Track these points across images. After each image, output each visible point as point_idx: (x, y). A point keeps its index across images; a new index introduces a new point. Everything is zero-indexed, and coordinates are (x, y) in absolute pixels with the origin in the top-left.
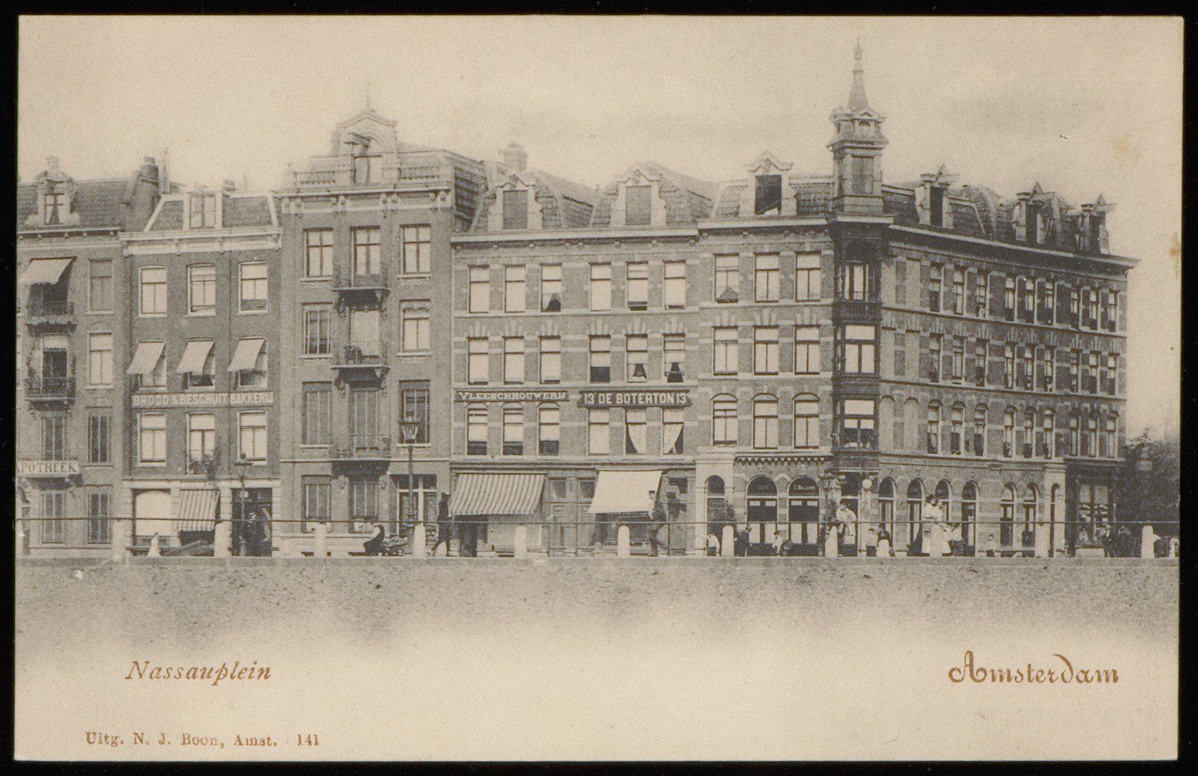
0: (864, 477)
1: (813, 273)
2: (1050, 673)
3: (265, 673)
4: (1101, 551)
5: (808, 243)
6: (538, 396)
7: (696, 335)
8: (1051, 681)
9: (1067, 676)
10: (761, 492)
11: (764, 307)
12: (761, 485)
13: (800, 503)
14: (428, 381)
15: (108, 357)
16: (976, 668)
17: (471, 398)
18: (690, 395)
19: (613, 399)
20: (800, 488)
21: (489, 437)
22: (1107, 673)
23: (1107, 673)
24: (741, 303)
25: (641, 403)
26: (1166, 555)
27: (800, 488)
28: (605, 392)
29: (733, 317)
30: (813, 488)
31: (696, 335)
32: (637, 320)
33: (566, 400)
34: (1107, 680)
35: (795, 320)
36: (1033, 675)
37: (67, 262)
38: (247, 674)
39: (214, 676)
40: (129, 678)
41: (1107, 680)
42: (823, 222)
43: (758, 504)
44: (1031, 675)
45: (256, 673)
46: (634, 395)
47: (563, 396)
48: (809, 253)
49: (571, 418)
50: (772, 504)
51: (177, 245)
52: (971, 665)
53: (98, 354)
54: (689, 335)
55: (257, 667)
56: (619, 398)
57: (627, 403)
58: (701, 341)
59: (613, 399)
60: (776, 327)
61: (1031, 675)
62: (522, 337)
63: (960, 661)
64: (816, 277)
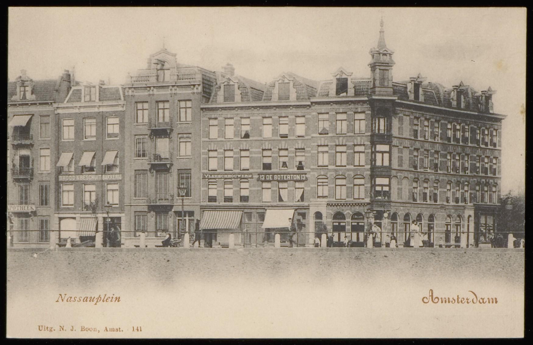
0: (384, 212)
2: (467, 299)
3: (118, 299)
4: (490, 245)
5: (360, 108)
6: (239, 176)
7: (310, 149)
8: (468, 303)
9: (475, 300)
10: (338, 219)
12: (339, 216)
13: (356, 224)
16: (434, 297)
18: (307, 176)
19: (273, 177)
20: (356, 217)
22: (492, 299)
23: (492, 299)
24: (330, 135)
25: (285, 179)
27: (356, 217)
28: (269, 174)
30: (362, 217)
31: (310, 149)
32: (283, 142)
33: (252, 178)
34: (493, 302)
36: (460, 300)
37: (30, 116)
38: (110, 299)
39: (95, 300)
40: (57, 301)
41: (493, 302)
44: (459, 300)
45: (114, 299)
46: (282, 175)
47: (250, 176)
49: (254, 186)
50: (344, 224)
52: (432, 296)
54: (306, 149)
55: (114, 297)
57: (279, 179)
58: (312, 152)
59: (273, 177)
60: (345, 145)
61: (459, 300)
62: (232, 150)
63: (427, 294)
64: (363, 123)
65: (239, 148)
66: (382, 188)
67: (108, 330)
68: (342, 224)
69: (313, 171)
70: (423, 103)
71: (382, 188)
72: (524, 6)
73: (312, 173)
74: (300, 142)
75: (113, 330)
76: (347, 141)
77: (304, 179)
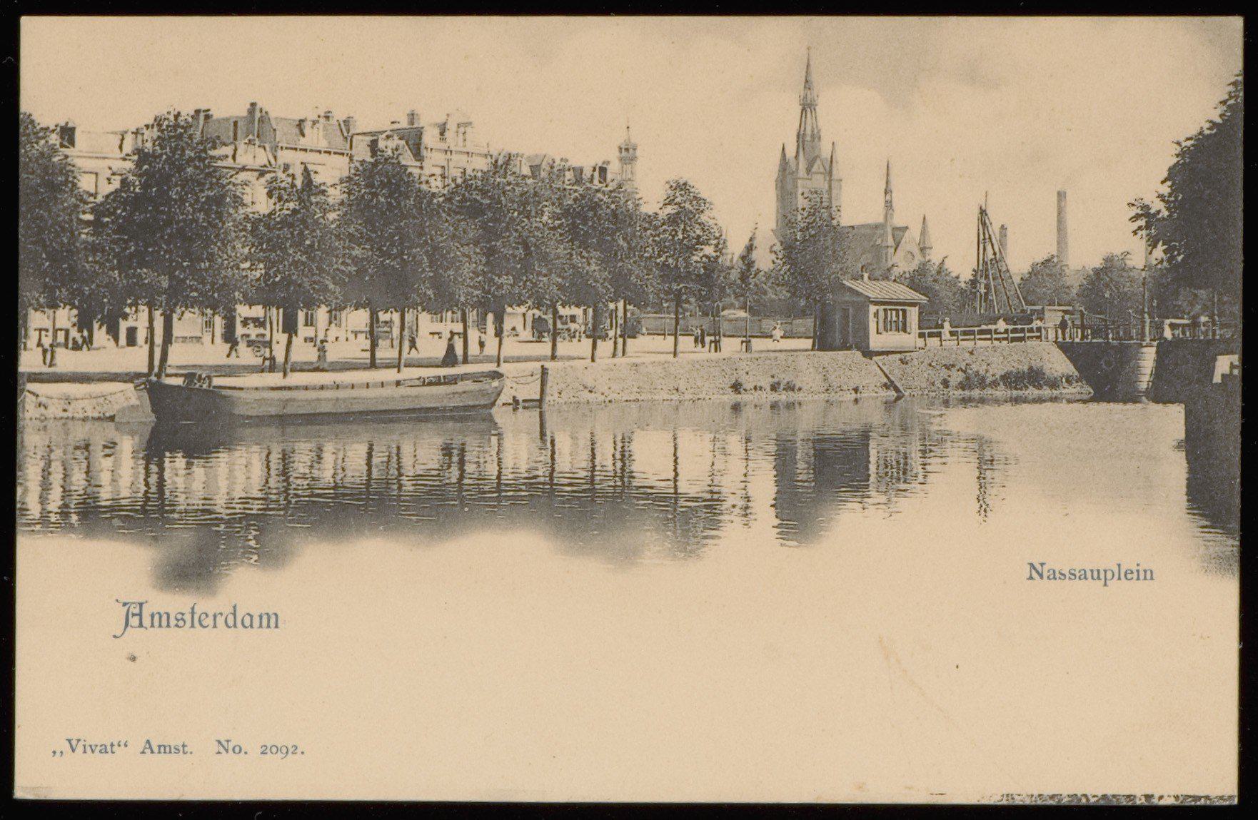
67: (156, 749)
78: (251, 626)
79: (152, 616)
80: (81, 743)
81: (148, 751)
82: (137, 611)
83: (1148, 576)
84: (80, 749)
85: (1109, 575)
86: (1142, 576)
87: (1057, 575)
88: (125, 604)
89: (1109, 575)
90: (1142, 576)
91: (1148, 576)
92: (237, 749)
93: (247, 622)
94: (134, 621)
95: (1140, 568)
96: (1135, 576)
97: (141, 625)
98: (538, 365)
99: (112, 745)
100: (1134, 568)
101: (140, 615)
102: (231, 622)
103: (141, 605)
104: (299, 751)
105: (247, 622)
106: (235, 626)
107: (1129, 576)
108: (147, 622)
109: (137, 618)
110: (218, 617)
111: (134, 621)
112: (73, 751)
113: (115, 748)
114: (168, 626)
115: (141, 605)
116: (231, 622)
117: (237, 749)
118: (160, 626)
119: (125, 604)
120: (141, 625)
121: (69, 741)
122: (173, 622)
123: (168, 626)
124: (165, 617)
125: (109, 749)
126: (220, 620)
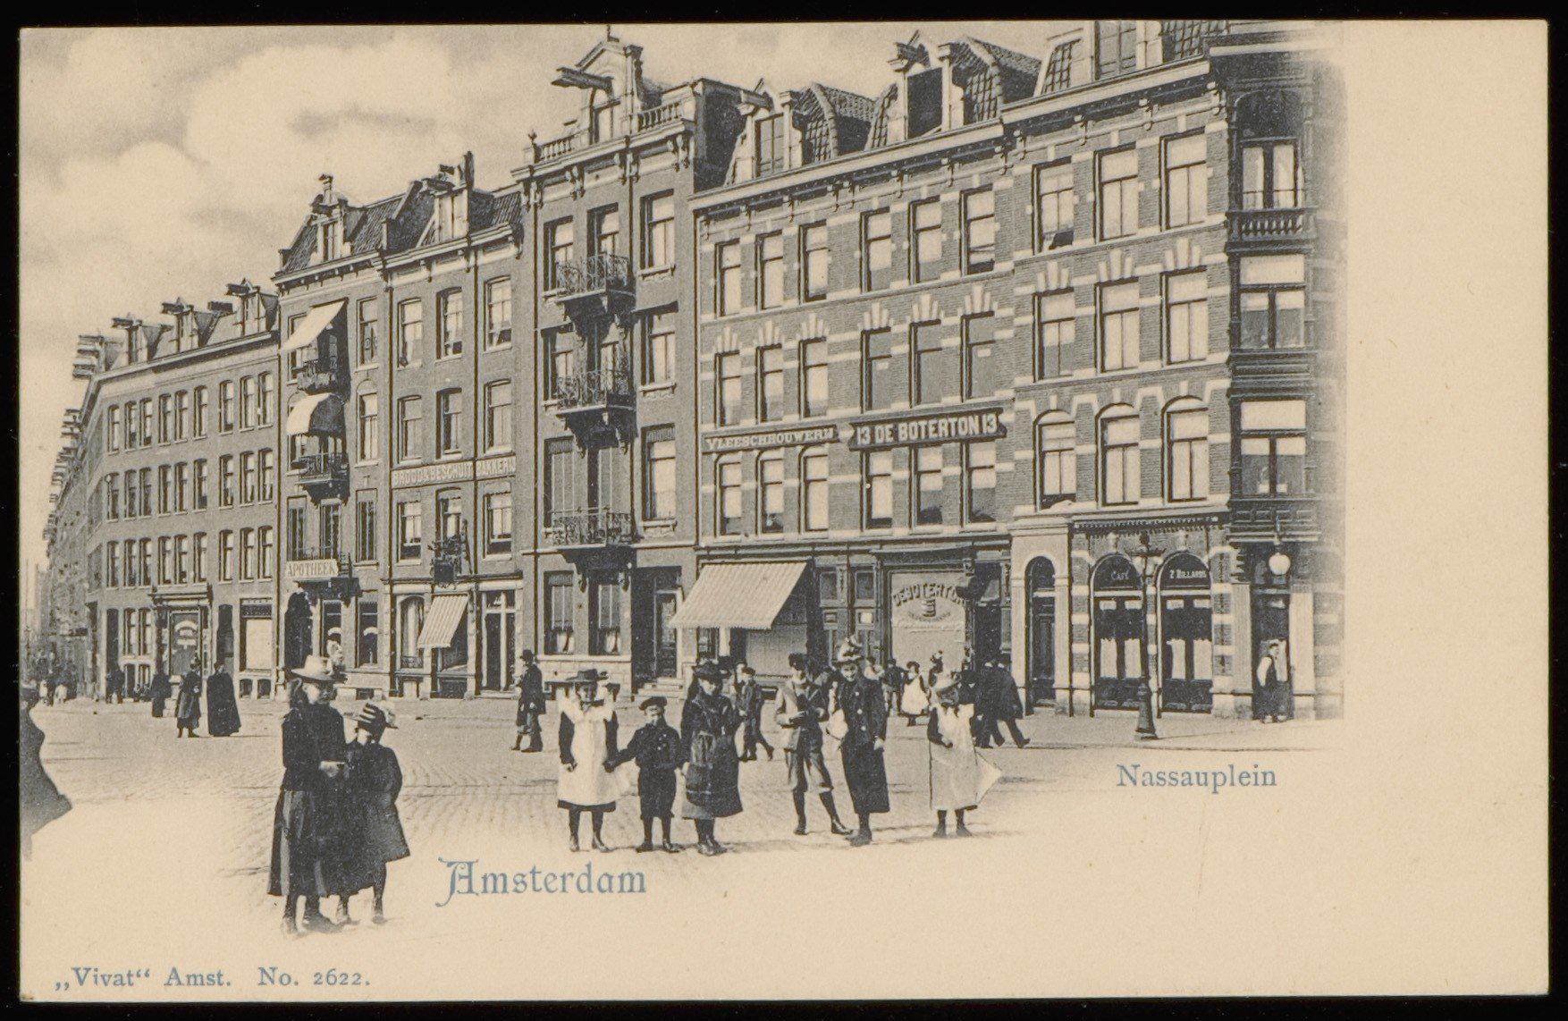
0: (1271, 550)
1: (1195, 171)
5: (1180, 115)
6: (798, 436)
7: (1008, 311)
10: (1117, 585)
11: (1112, 247)
12: (1111, 573)
13: (1180, 603)
14: (671, 426)
15: (1201, 312)
17: (720, 447)
18: (1004, 418)
19: (895, 433)
20: (1180, 574)
21: (1078, 486)
24: (1077, 245)
25: (932, 436)
26: (260, 681)
27: (1180, 574)
28: (883, 422)
29: (1196, 250)
30: (1201, 574)
31: (1008, 311)
32: (978, 289)
33: (835, 440)
35: (1163, 262)
37: (340, 305)
42: (1203, 68)
43: (1112, 605)
46: (923, 423)
47: (829, 434)
48: (1186, 134)
49: (841, 469)
50: (1205, 604)
51: (467, 256)
53: (1117, 318)
54: (999, 313)
56: (904, 432)
57: (914, 437)
58: (1018, 321)
59: (895, 433)
60: (1134, 279)
62: (780, 346)
64: (1201, 176)
65: (960, 312)
66: (1273, 447)
67: (183, 979)
68: (1198, 604)
69: (1022, 398)
70: (349, 258)
71: (1273, 447)
72: (17, 35)
73: (1019, 405)
74: (925, 298)
75: (194, 979)
76: (1141, 261)
77: (993, 430)
78: (610, 890)
79: (485, 878)
80: (91, 973)
81: (174, 982)
82: (465, 872)
83: (1269, 780)
84: (90, 979)
85: (1220, 779)
86: (1260, 781)
87: (1155, 779)
88: (450, 864)
89: (1220, 779)
90: (1260, 781)
91: (1269, 780)
92: (285, 980)
93: (605, 885)
94: (462, 885)
95: (1259, 770)
96: (1252, 779)
97: (470, 891)
98: (444, 458)
99: (129, 975)
100: (1251, 770)
101: (469, 877)
102: (584, 886)
103: (470, 864)
104: (363, 980)
105: (605, 885)
106: (589, 890)
107: (1245, 781)
108: (478, 884)
109: (466, 881)
110: (569, 879)
111: (462, 885)
112: (81, 982)
113: (133, 979)
114: (505, 891)
115: (470, 864)
116: (584, 886)
117: (285, 980)
118: (495, 891)
119: (450, 864)
120: (470, 891)
121: (77, 970)
122: (511, 886)
123: (505, 891)
124: (500, 880)
125: (125, 980)
126: (571, 882)
